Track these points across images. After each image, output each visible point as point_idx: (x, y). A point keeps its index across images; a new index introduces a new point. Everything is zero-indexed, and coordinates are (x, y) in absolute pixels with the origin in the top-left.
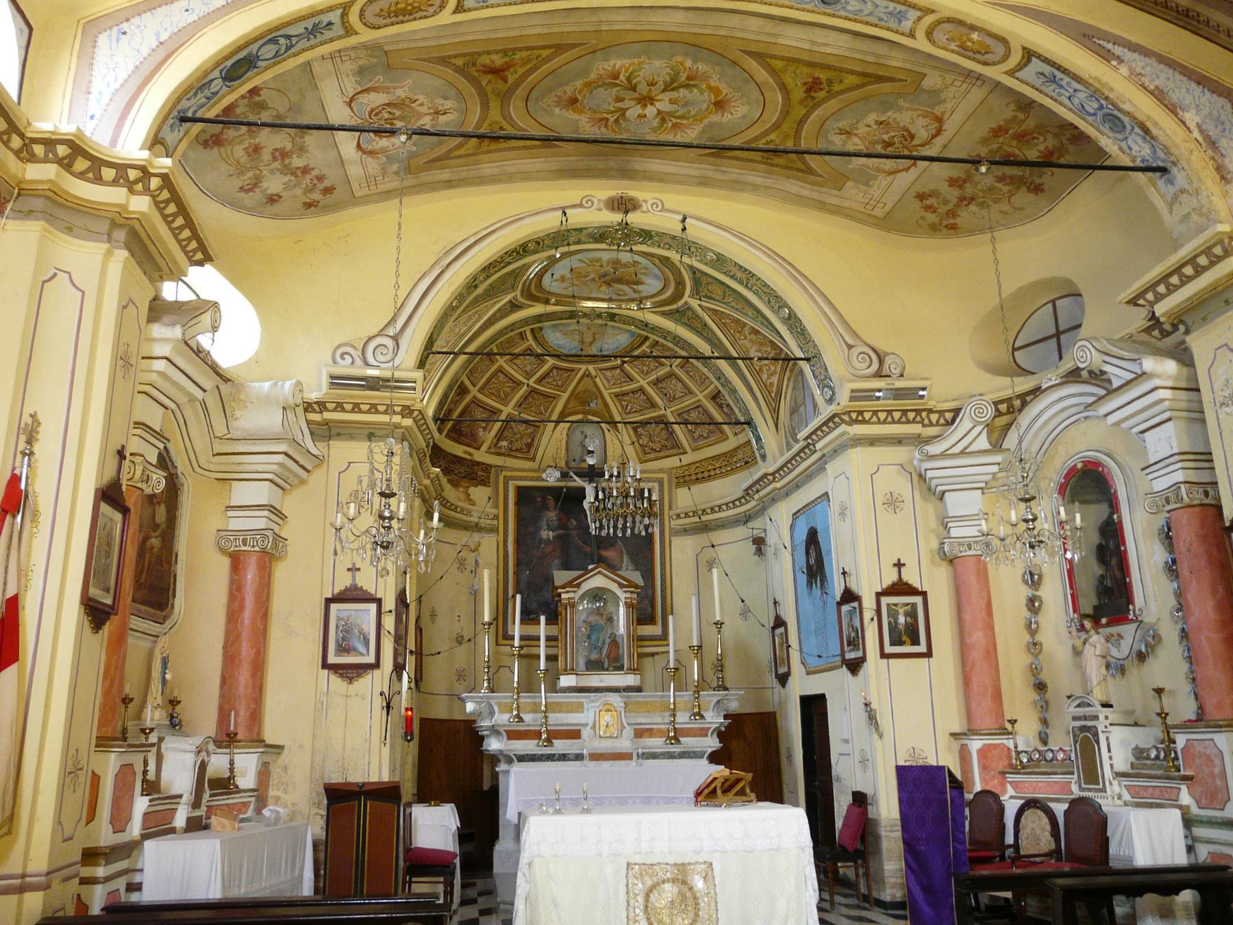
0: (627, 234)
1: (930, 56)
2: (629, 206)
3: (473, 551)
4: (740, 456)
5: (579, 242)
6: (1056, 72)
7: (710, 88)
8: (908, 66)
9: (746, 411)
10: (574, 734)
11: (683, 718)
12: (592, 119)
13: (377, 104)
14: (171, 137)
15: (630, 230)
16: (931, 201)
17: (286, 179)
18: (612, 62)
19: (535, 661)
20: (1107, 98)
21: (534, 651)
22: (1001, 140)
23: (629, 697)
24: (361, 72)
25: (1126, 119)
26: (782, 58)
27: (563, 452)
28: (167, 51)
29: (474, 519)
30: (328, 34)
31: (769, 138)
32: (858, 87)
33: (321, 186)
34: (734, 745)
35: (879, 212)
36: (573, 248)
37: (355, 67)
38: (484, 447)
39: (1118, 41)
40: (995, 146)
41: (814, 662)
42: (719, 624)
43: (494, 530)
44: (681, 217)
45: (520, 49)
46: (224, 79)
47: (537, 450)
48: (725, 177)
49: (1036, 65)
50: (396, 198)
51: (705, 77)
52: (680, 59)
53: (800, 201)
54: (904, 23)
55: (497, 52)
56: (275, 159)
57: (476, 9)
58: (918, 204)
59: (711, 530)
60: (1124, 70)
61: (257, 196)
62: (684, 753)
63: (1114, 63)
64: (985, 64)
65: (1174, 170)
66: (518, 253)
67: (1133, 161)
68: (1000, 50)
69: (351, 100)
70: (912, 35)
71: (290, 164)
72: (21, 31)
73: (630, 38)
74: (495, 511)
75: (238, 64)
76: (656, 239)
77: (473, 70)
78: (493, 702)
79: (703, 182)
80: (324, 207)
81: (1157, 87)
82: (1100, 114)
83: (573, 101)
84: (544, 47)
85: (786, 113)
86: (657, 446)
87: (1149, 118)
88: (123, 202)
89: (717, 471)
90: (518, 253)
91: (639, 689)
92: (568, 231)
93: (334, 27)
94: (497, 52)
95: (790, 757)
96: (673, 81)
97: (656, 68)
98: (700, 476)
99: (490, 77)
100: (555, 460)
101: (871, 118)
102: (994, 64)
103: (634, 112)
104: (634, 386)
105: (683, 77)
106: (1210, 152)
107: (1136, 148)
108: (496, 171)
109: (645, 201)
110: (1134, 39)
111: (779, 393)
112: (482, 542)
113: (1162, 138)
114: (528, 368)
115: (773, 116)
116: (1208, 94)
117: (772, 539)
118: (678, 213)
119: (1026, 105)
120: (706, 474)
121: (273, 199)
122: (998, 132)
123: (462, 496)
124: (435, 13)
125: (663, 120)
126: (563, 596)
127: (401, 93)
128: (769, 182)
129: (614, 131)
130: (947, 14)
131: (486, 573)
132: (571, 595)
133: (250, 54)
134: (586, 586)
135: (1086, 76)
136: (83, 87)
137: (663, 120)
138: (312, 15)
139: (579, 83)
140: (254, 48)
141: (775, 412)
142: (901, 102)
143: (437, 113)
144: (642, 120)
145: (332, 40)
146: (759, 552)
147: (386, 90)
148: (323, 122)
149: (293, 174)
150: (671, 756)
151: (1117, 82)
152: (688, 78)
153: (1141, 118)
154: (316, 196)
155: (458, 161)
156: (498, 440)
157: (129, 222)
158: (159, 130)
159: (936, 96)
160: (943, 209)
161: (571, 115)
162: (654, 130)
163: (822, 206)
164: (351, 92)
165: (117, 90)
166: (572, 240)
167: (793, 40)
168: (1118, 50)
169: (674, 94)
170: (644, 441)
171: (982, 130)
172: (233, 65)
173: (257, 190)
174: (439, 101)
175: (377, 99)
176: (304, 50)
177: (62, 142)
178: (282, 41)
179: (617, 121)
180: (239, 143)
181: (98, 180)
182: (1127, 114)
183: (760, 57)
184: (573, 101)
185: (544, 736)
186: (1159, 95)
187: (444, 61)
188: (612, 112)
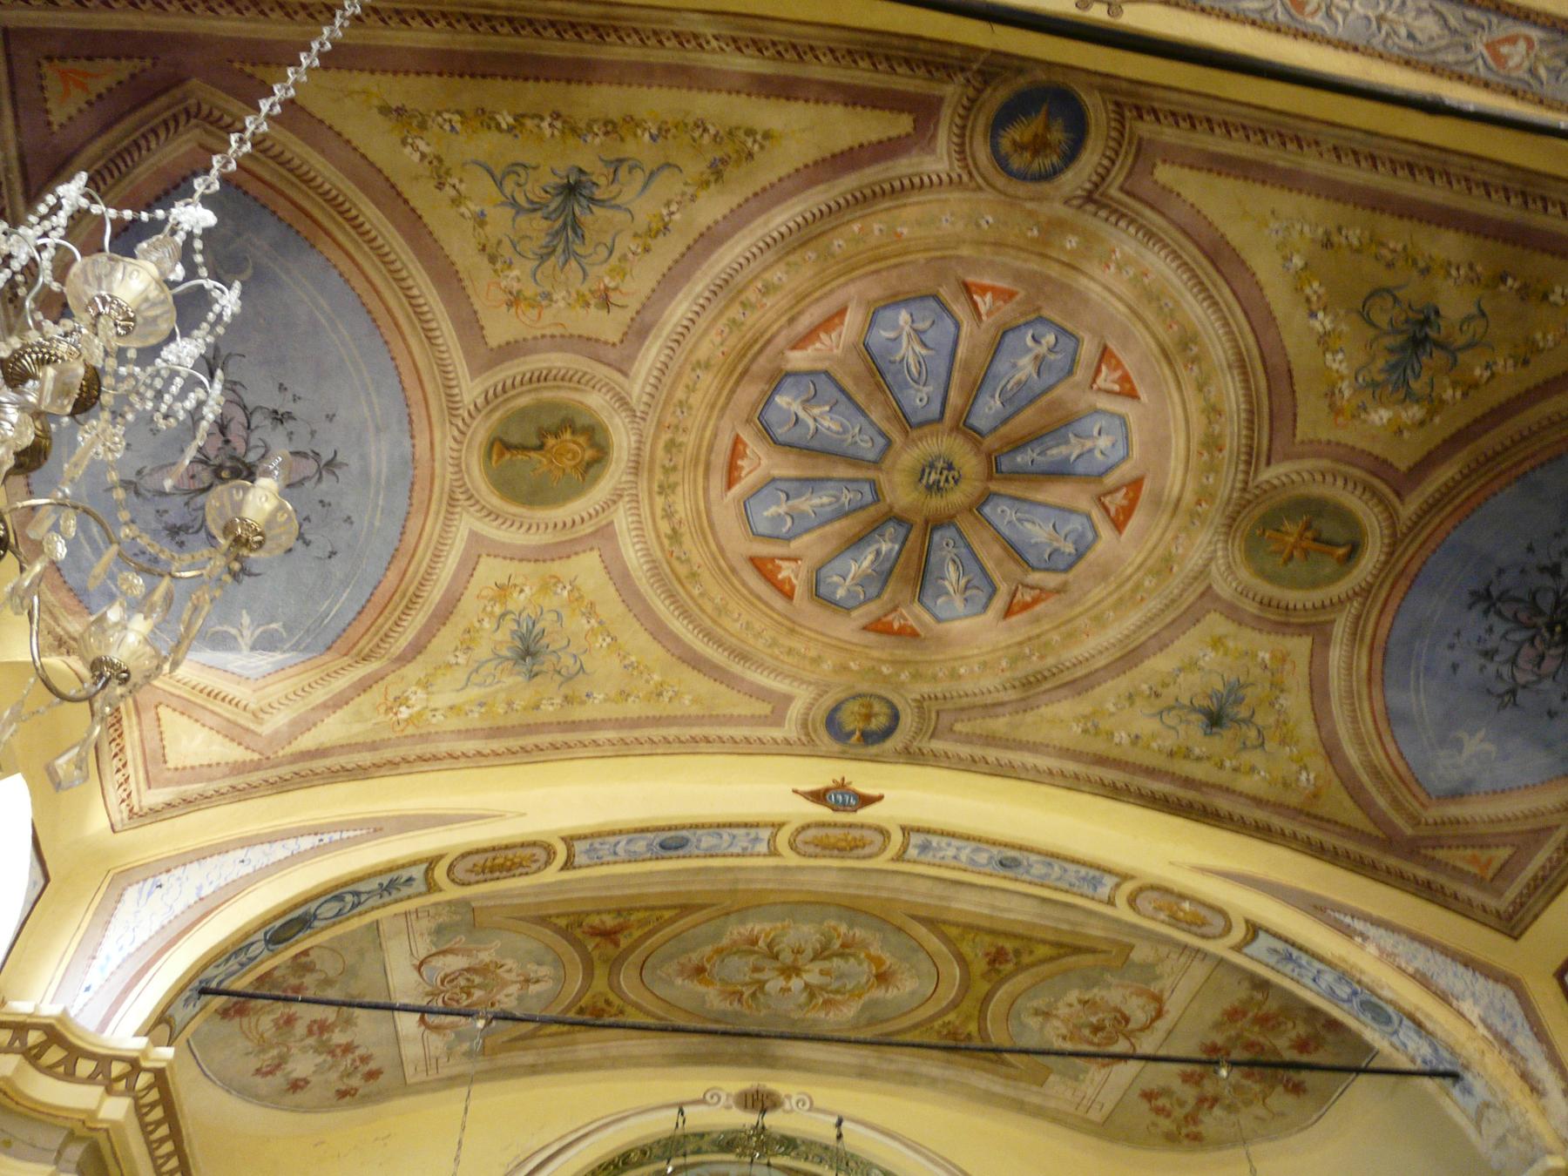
0: (764, 1142)
1: (1134, 927)
2: (767, 1103)
5: (698, 1151)
6: (1291, 949)
7: (870, 958)
8: (1112, 935)
12: (722, 992)
13: (454, 968)
14: (180, 1014)
15: (769, 1136)
16: (1161, 1102)
17: (320, 1059)
18: (749, 926)
20: (1359, 982)
22: (1239, 1025)
24: (439, 931)
25: (1390, 1009)
26: (957, 925)
28: (206, 909)
30: (406, 891)
31: (946, 1019)
32: (1052, 959)
33: (366, 1069)
35: (1096, 1115)
36: (690, 1159)
37: (433, 925)
39: (1355, 914)
40: (1233, 1033)
44: (835, 1120)
45: (638, 909)
46: (268, 942)
48: (893, 1067)
49: (1263, 941)
50: (462, 1084)
51: (864, 945)
52: (833, 923)
53: (989, 1098)
54: (1100, 890)
55: (609, 912)
56: (310, 1032)
57: (588, 866)
58: (1145, 1106)
60: (1371, 949)
61: (278, 1080)
63: (1358, 940)
65: (1468, 1077)
66: (616, 1166)
67: (1413, 1060)
68: (1219, 923)
69: (421, 964)
70: (1111, 902)
71: (329, 1039)
72: (35, 883)
73: (772, 899)
75: (288, 926)
76: (803, 1148)
77: (578, 933)
79: (864, 1073)
80: (364, 1096)
81: (1417, 970)
82: (1355, 1001)
83: (699, 971)
84: (667, 908)
85: (966, 986)
87: (1418, 1008)
88: (92, 1105)
90: (616, 1166)
92: (685, 1136)
93: (415, 884)
94: (609, 912)
96: (824, 949)
97: (805, 933)
99: (598, 939)
101: (1073, 996)
102: (1214, 937)
103: (775, 984)
105: (837, 944)
106: (1505, 1053)
107: (1411, 1046)
108: (597, 1054)
109: (789, 1097)
110: (1376, 912)
113: (1440, 1033)
115: (949, 993)
116: (1481, 980)
118: (832, 1114)
119: (1262, 985)
121: (296, 1085)
122: (1234, 1015)
124: (539, 870)
125: (812, 996)
127: (485, 956)
128: (950, 1073)
129: (749, 1007)
130: (1149, 881)
133: (306, 913)
135: (1329, 956)
136: (89, 950)
137: (812, 996)
138: (391, 870)
139: (708, 950)
140: (313, 906)
142: (1108, 976)
143: (527, 981)
144: (786, 995)
145: (409, 897)
147: (467, 953)
148: (382, 1000)
149: (332, 1053)
151: (1366, 960)
152: (843, 946)
153: (1408, 1007)
154: (356, 1082)
155: (549, 1040)
157: (94, 1134)
158: (169, 1005)
159: (1148, 971)
160: (1179, 1113)
161: (697, 987)
162: (801, 1007)
163: (1020, 1107)
164: (423, 954)
165: (130, 955)
166: (690, 1148)
167: (967, 905)
168: (1359, 925)
169: (826, 965)
171: (1213, 1013)
172: (282, 926)
173: (279, 1074)
174: (532, 967)
175: (455, 963)
176: (373, 909)
177: (36, 1027)
178: (349, 898)
179: (754, 994)
180: (266, 1019)
181: (70, 1076)
182: (1390, 1002)
183: (931, 923)
184: (699, 971)
186: (1422, 980)
187: (543, 920)
188: (746, 984)
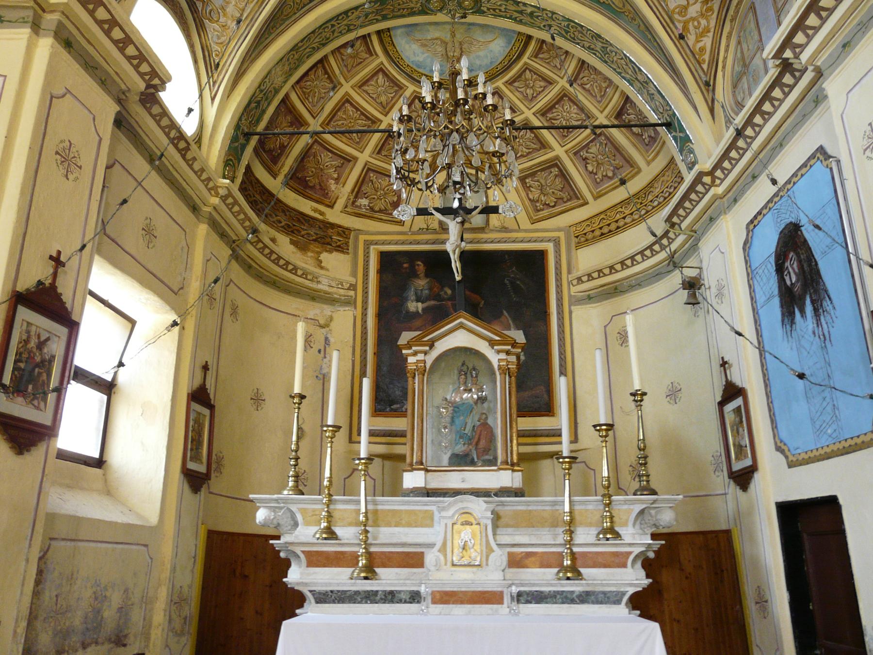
3: (322, 327)
4: (657, 191)
9: (664, 107)
10: (412, 559)
11: (586, 537)
23: (503, 504)
29: (323, 287)
34: (666, 577)
38: (339, 205)
41: (803, 442)
42: (638, 397)
43: (350, 302)
59: (623, 292)
62: (588, 593)
64: (753, 224)
74: (352, 280)
86: (551, 200)
89: (628, 220)
91: (518, 493)
95: (763, 602)
98: (605, 230)
111: (714, 61)
112: (335, 316)
114: (383, 99)
117: (710, 279)
120: (613, 226)
123: (311, 261)
126: (411, 360)
131: (335, 355)
132: (420, 357)
134: (442, 346)
141: (708, 86)
146: (693, 302)
150: (567, 598)
156: (356, 197)
170: (535, 194)
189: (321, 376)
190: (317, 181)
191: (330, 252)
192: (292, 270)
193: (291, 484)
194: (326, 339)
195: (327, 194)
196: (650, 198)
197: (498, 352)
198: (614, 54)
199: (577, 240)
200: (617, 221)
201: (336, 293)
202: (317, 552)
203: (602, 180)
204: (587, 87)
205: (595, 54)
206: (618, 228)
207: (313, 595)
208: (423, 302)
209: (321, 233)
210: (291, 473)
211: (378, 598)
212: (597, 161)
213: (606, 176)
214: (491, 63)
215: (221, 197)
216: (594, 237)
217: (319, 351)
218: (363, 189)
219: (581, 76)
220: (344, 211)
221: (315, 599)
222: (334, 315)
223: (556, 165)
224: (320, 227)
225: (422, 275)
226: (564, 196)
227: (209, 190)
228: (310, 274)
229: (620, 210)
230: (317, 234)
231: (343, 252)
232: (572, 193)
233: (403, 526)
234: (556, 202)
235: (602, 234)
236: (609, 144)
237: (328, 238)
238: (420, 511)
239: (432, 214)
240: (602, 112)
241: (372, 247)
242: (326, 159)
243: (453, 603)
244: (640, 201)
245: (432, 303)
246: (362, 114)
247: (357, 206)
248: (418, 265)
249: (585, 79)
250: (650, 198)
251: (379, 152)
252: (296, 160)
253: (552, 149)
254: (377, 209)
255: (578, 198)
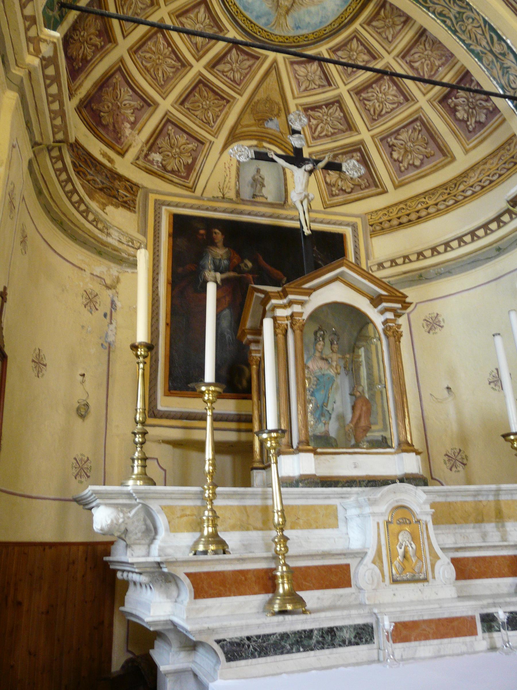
3: (108, 287)
4: (471, 181)
10: (335, 576)
19: (194, 455)
21: (196, 435)
27: (233, 180)
47: (198, 177)
59: (428, 279)
78: (155, 506)
98: (404, 219)
100: (221, 189)
104: (330, 94)
112: (122, 277)
185: (284, 587)
189: (106, 345)
190: (111, 120)
191: (117, 206)
192: (84, 211)
193: (137, 470)
194: (113, 302)
195: (120, 138)
196: (462, 187)
197: (382, 312)
198: (471, 20)
199: (371, 228)
200: (418, 212)
201: (125, 252)
202: (208, 574)
203: (406, 169)
204: (416, 65)
205: (444, 22)
206: (419, 217)
207: (222, 647)
208: (221, 273)
209: (107, 183)
210: (137, 454)
211: (314, 641)
212: (405, 148)
213: (413, 165)
214: (321, 23)
215: (43, 59)
216: (391, 226)
217: (105, 315)
218: (158, 142)
219: (412, 52)
220: (135, 163)
221: (226, 654)
222: (121, 277)
223: (359, 150)
224: (106, 176)
225: (220, 244)
226: (362, 183)
227: (29, 40)
228: (102, 221)
229: (424, 200)
230: (103, 183)
231: (129, 209)
232: (371, 180)
233: (302, 528)
234: (352, 189)
235: (400, 224)
236: (424, 130)
237: (117, 190)
238: (321, 506)
239: (273, 160)
240: (424, 95)
241: (164, 208)
242: (126, 96)
243: (415, 640)
244: (448, 191)
245: (231, 274)
246: (173, 51)
247: (149, 161)
248: (215, 233)
249: (416, 56)
250: (462, 187)
251: (182, 103)
252: (95, 84)
253: (359, 133)
254: (169, 168)
255: (377, 186)
